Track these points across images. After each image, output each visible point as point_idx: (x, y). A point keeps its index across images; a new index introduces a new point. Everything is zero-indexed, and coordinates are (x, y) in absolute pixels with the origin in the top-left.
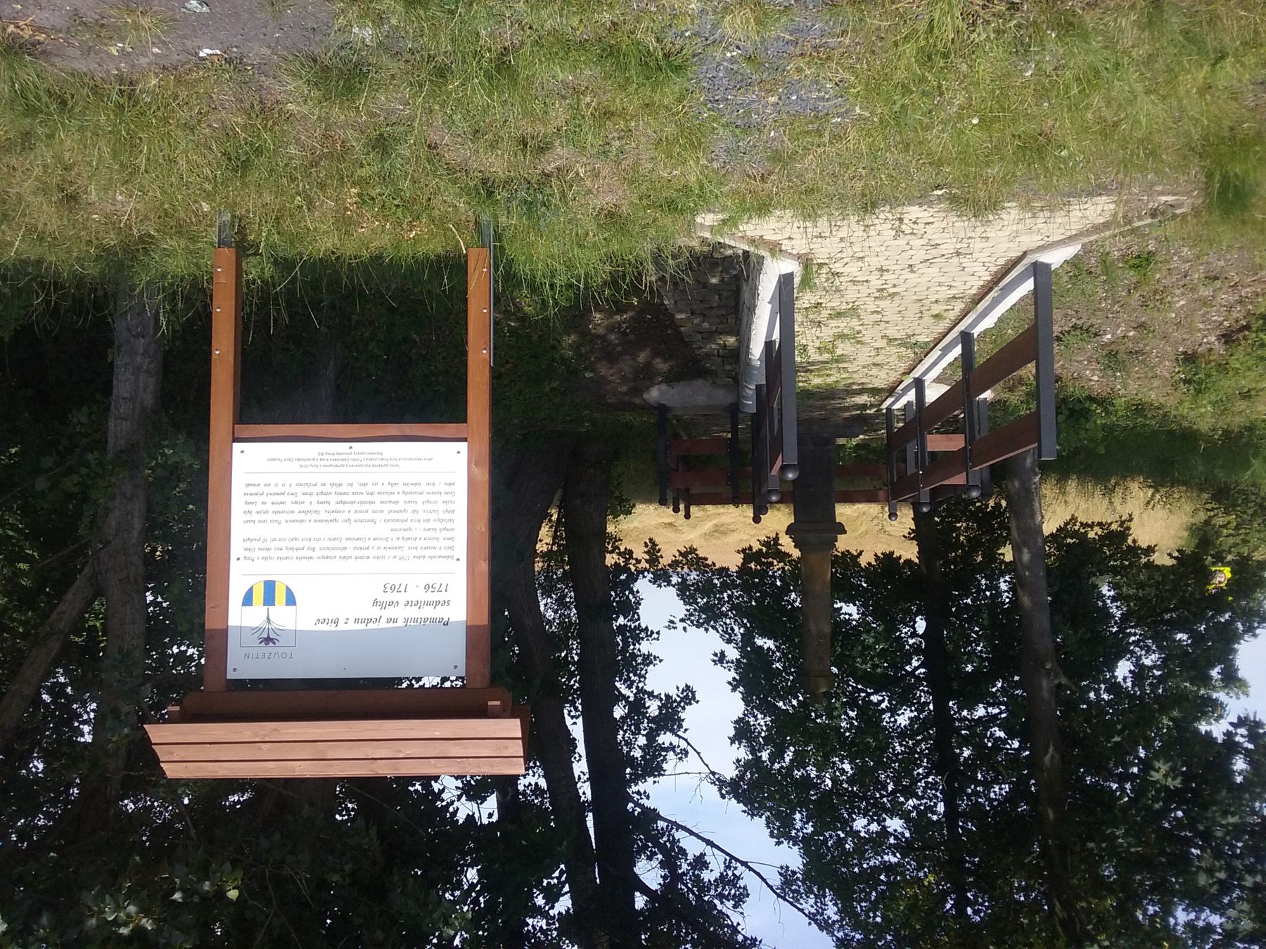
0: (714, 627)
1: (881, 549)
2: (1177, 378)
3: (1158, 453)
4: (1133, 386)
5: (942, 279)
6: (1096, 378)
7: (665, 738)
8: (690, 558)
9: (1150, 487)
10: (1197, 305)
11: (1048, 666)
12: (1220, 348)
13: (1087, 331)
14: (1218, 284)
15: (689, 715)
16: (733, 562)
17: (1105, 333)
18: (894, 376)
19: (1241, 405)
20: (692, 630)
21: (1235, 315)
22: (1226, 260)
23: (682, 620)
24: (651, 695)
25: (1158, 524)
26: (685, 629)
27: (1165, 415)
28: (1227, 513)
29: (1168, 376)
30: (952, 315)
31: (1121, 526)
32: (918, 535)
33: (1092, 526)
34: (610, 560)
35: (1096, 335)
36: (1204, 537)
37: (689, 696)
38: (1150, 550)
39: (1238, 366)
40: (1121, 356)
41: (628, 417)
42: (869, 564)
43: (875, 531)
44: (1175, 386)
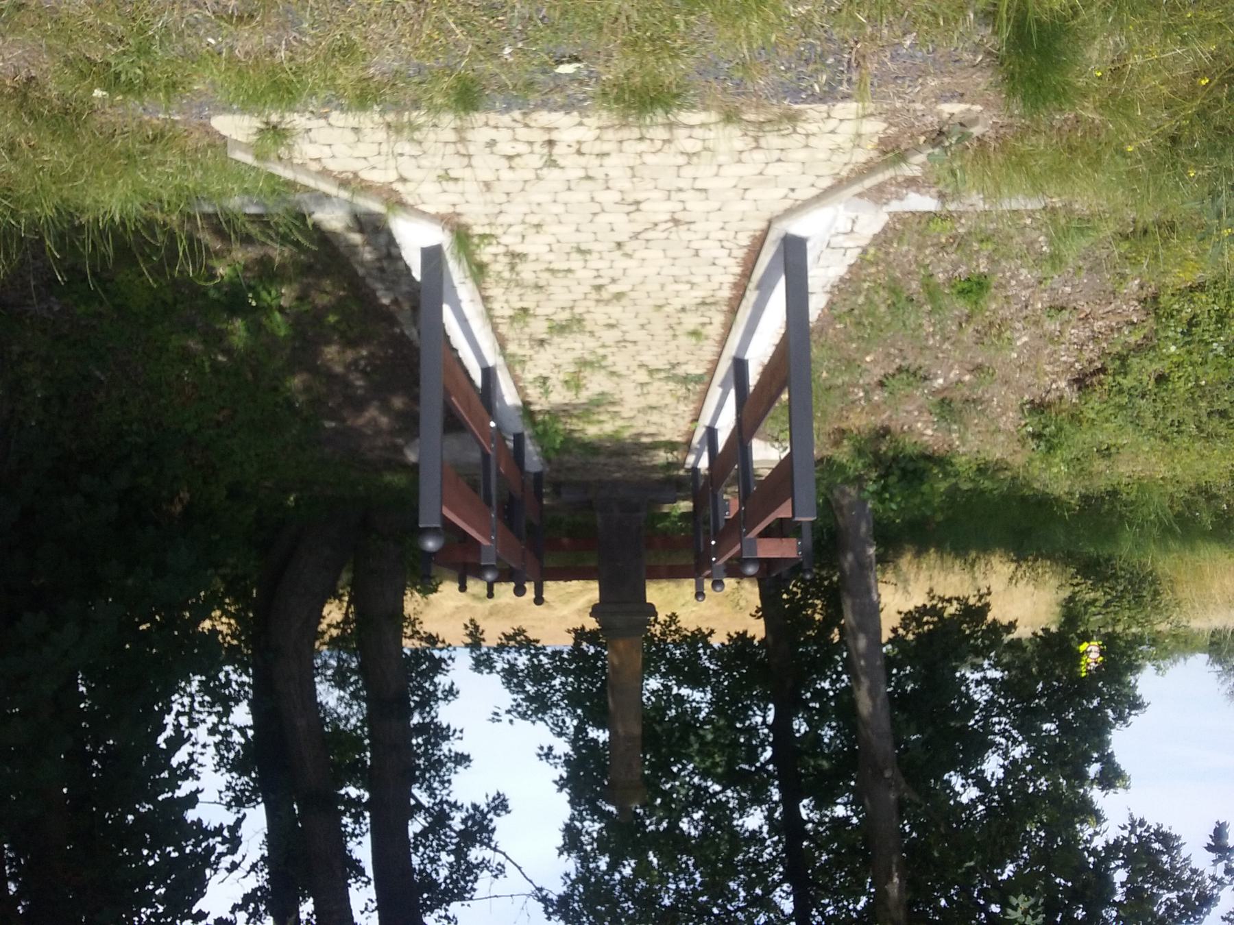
0: (542, 719)
1: (736, 628)
2: (1023, 431)
3: (1010, 521)
4: (973, 442)
5: (675, 271)
6: (929, 432)
7: (476, 854)
8: (518, 640)
9: (1012, 561)
10: (1041, 343)
11: (888, 774)
12: (1072, 395)
13: (915, 374)
14: (1065, 314)
15: (500, 823)
16: (565, 643)
17: (936, 377)
18: (684, 425)
19: (1099, 465)
20: (519, 722)
21: (1087, 355)
22: (1073, 287)
23: (509, 712)
24: (455, 806)
25: (1024, 601)
26: (511, 721)
27: (1014, 478)
28: (1094, 588)
29: (1012, 429)
30: (715, 331)
31: (980, 600)
32: (768, 609)
33: (949, 601)
34: (408, 645)
35: (925, 378)
36: (1072, 614)
37: (500, 805)
38: (1012, 626)
39: (1093, 416)
40: (957, 405)
41: (388, 477)
42: (723, 644)
43: (721, 611)
44: (1022, 442)
